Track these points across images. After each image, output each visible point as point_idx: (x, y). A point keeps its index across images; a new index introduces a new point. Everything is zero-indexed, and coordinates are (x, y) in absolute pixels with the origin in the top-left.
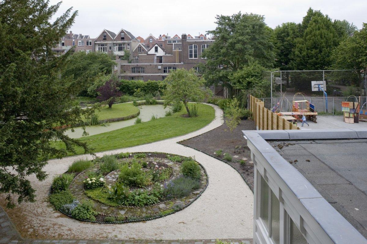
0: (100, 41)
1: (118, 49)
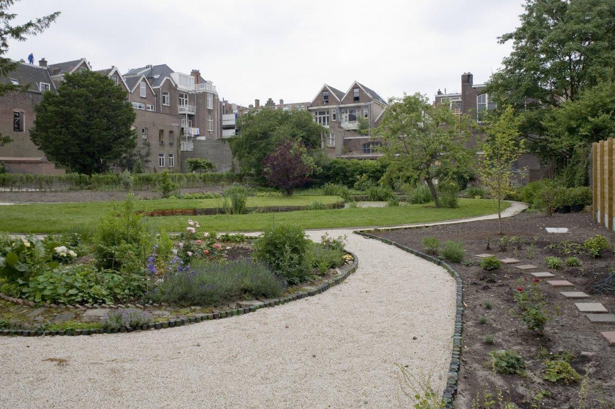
0: (318, 106)
1: (348, 118)
